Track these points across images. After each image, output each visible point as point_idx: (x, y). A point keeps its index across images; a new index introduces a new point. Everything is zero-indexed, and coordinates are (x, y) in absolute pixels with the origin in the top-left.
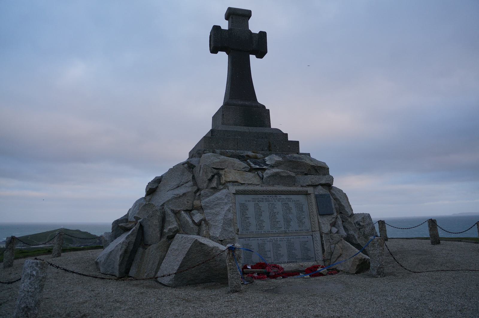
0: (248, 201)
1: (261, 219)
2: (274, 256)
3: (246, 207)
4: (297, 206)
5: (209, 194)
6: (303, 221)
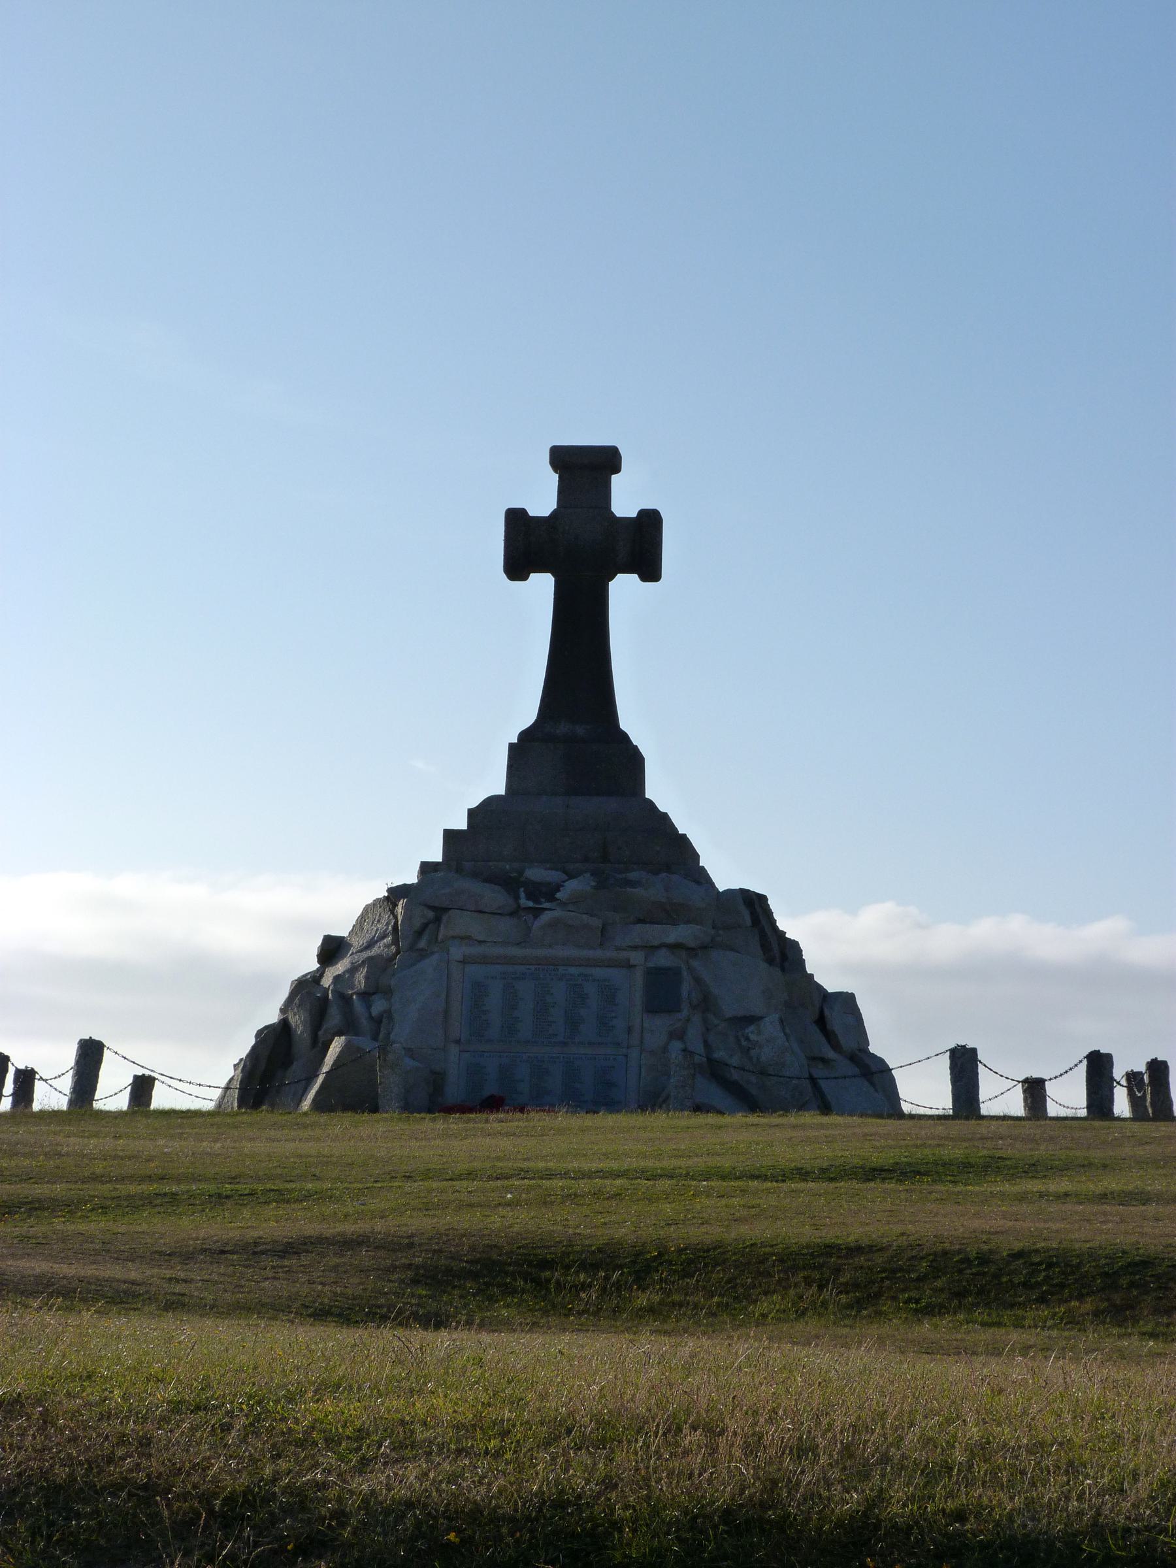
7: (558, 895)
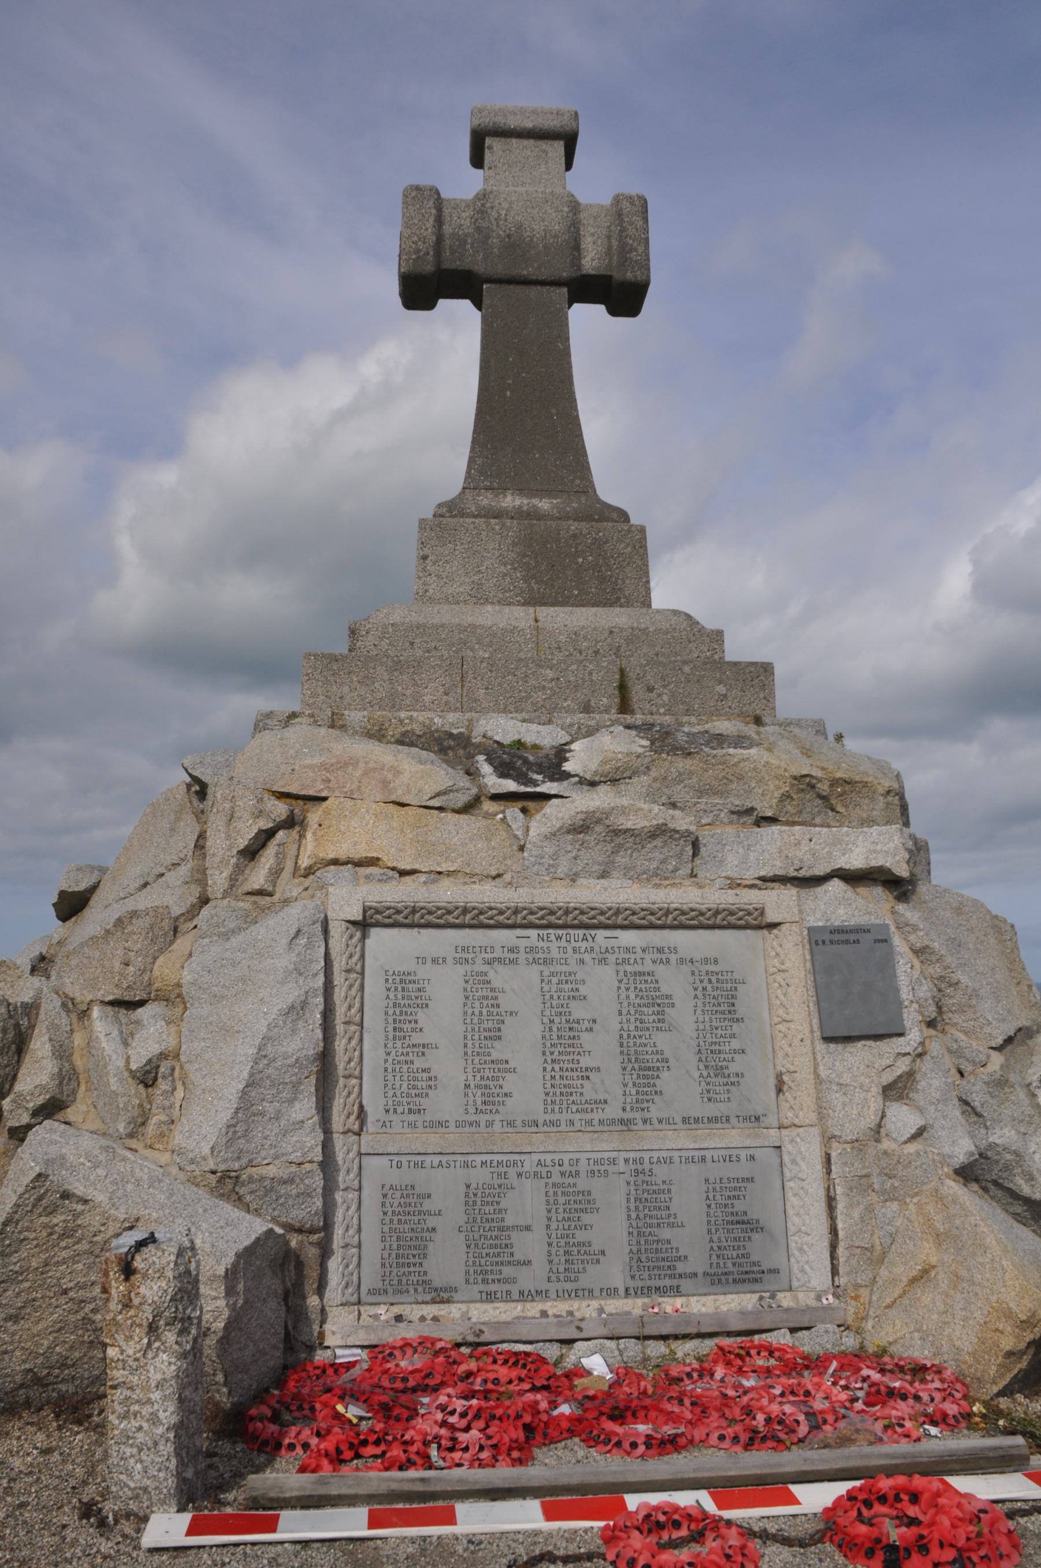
0: (435, 961)
1: (495, 1055)
2: (550, 1254)
3: (419, 990)
4: (705, 989)
5: (232, 926)
6: (733, 1068)
7: (567, 767)
